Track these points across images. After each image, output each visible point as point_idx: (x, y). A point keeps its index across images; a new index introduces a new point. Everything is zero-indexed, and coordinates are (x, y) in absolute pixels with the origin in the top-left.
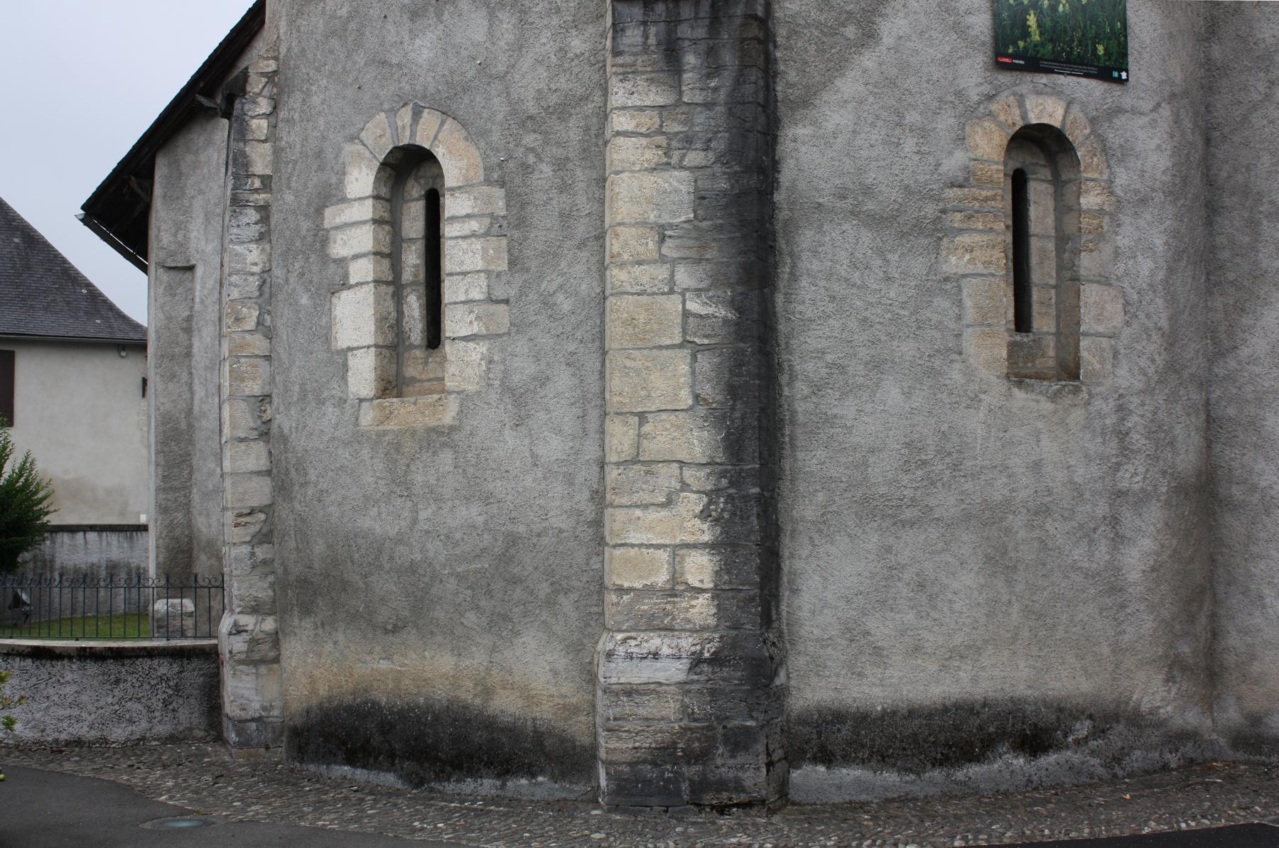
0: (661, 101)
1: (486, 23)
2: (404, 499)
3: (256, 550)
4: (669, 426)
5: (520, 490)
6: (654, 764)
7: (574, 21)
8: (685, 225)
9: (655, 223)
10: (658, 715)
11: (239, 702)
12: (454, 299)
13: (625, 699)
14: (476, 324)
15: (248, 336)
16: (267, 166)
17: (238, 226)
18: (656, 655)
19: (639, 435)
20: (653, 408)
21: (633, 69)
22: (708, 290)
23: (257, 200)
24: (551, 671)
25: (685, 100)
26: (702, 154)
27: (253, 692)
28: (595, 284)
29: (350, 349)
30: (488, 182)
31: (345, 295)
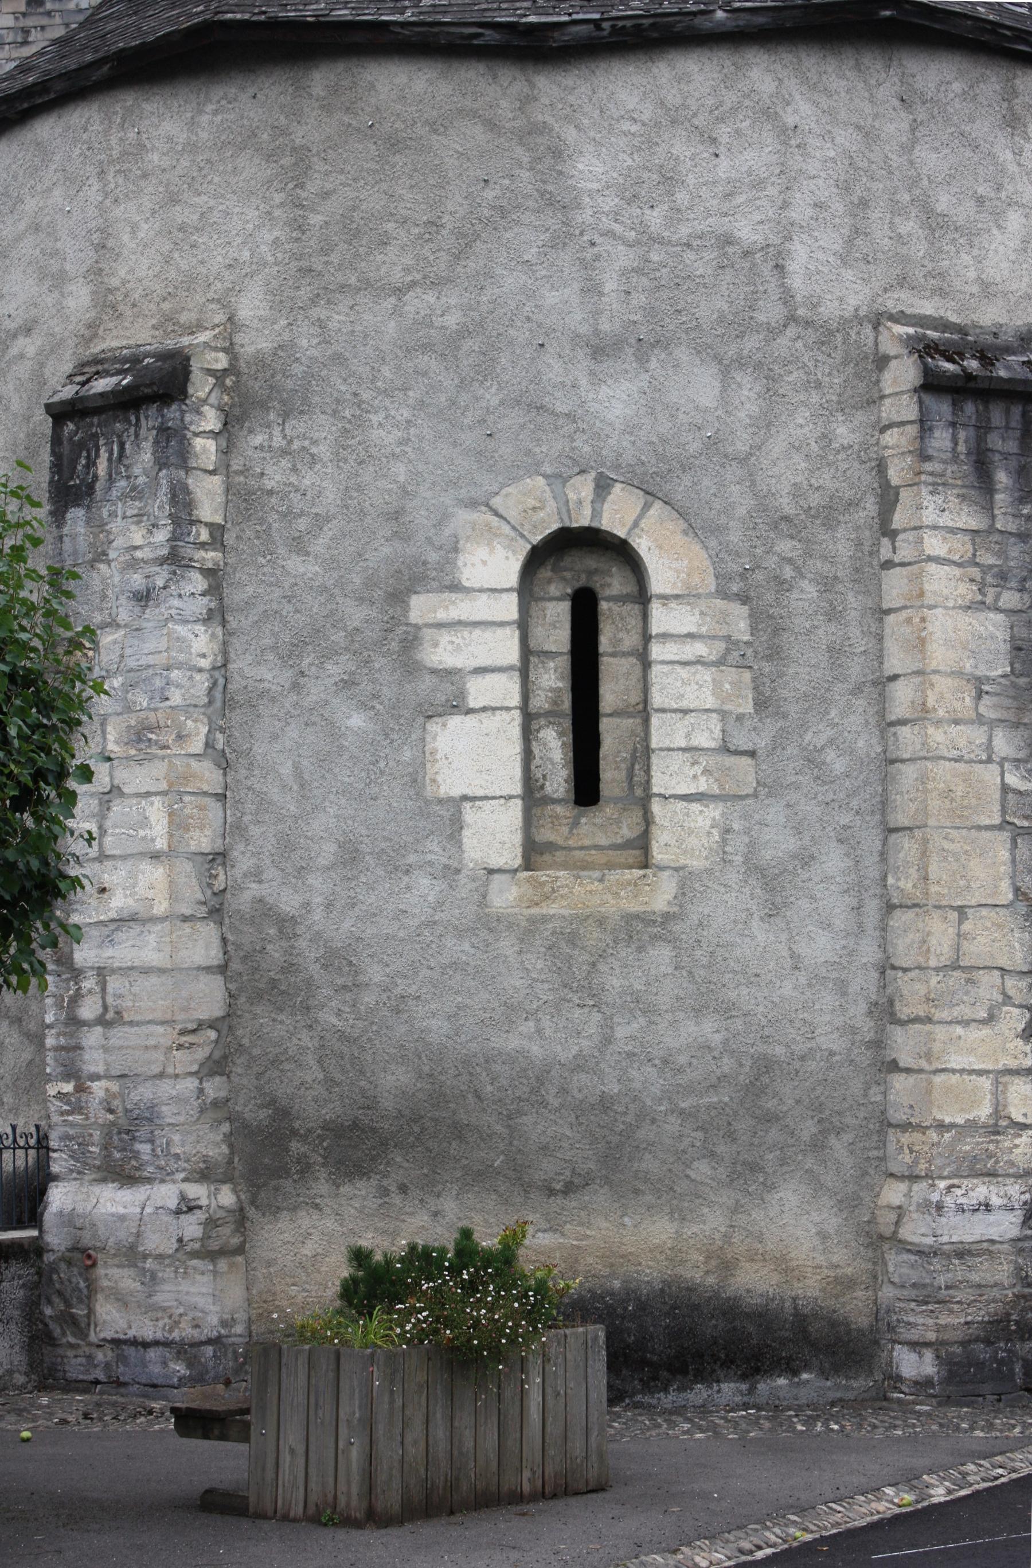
0: (973, 524)
1: (717, 384)
2: (586, 1010)
3: (205, 1085)
4: (989, 925)
5: (777, 1000)
6: (988, 1342)
7: (839, 403)
8: (1002, 680)
9: (972, 674)
10: (991, 1281)
11: (191, 1315)
12: (667, 743)
13: (957, 1262)
14: (703, 779)
15: (194, 763)
16: (216, 511)
17: (180, 596)
18: (987, 1207)
19: (959, 935)
20: (973, 902)
21: (943, 479)
22: (1026, 761)
23: (204, 559)
24: (818, 1234)
25: (998, 526)
26: (1018, 595)
27: (210, 1300)
28: (874, 741)
29: (465, 798)
30: (722, 593)
31: (455, 721)
